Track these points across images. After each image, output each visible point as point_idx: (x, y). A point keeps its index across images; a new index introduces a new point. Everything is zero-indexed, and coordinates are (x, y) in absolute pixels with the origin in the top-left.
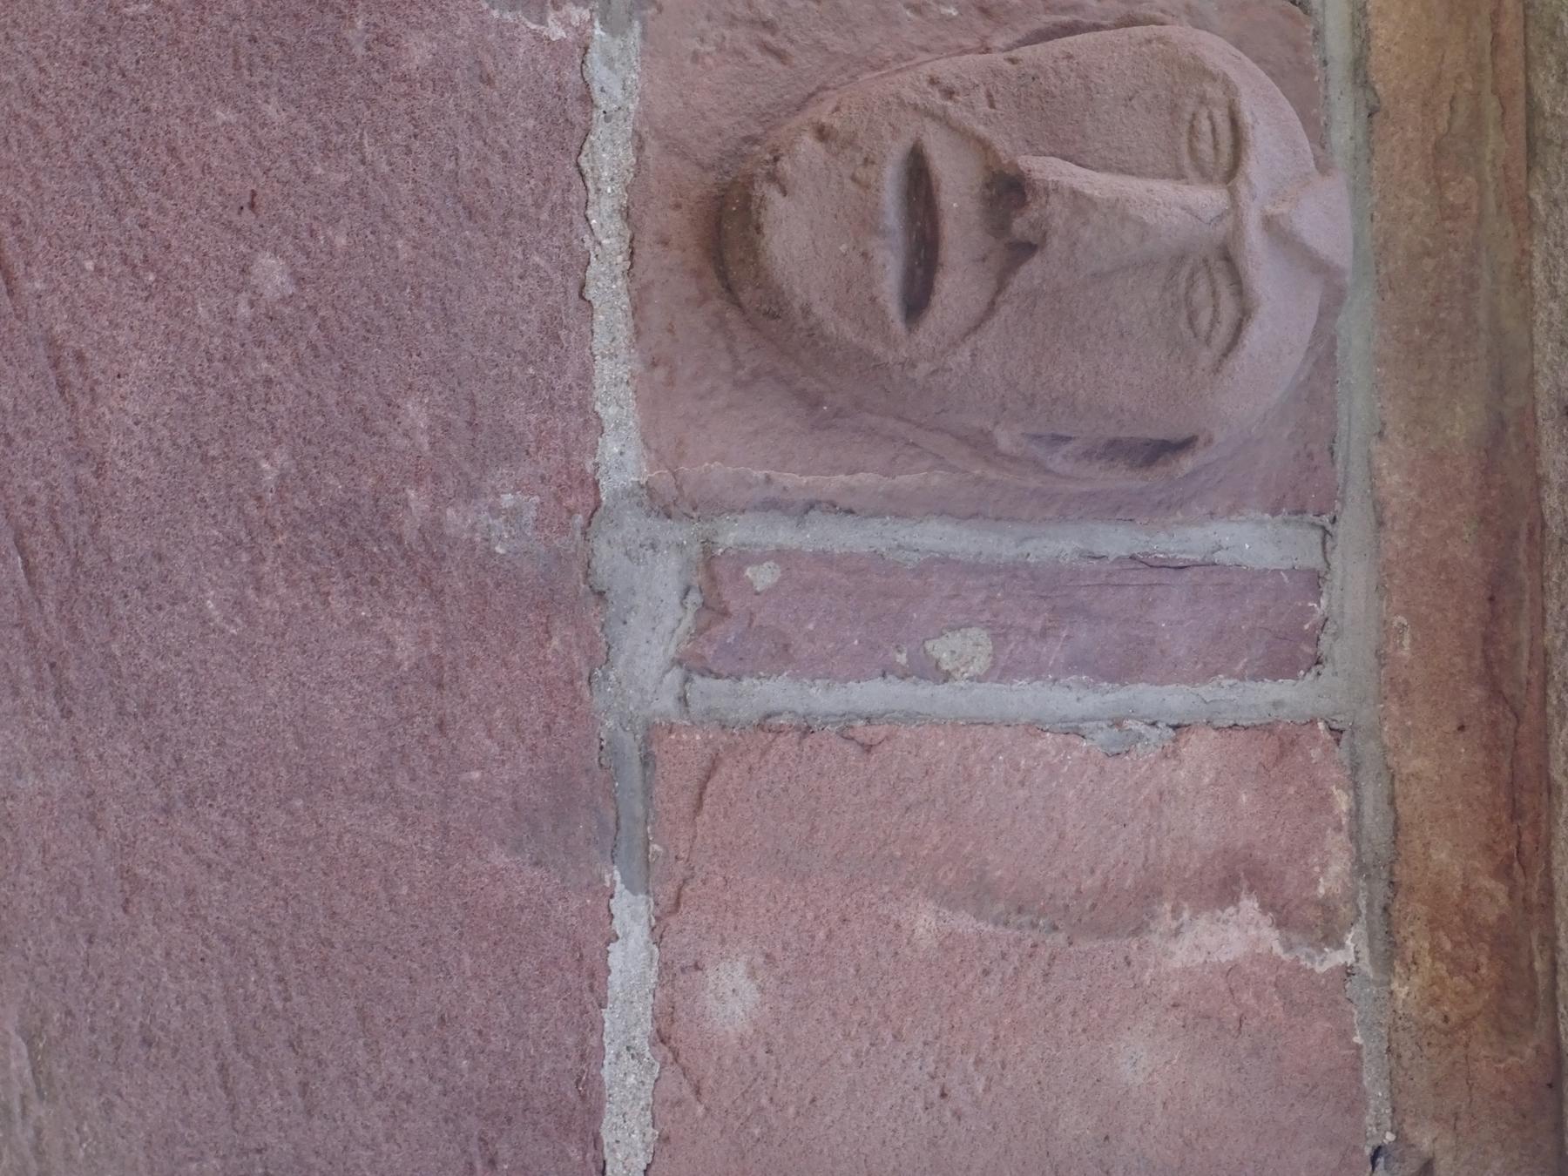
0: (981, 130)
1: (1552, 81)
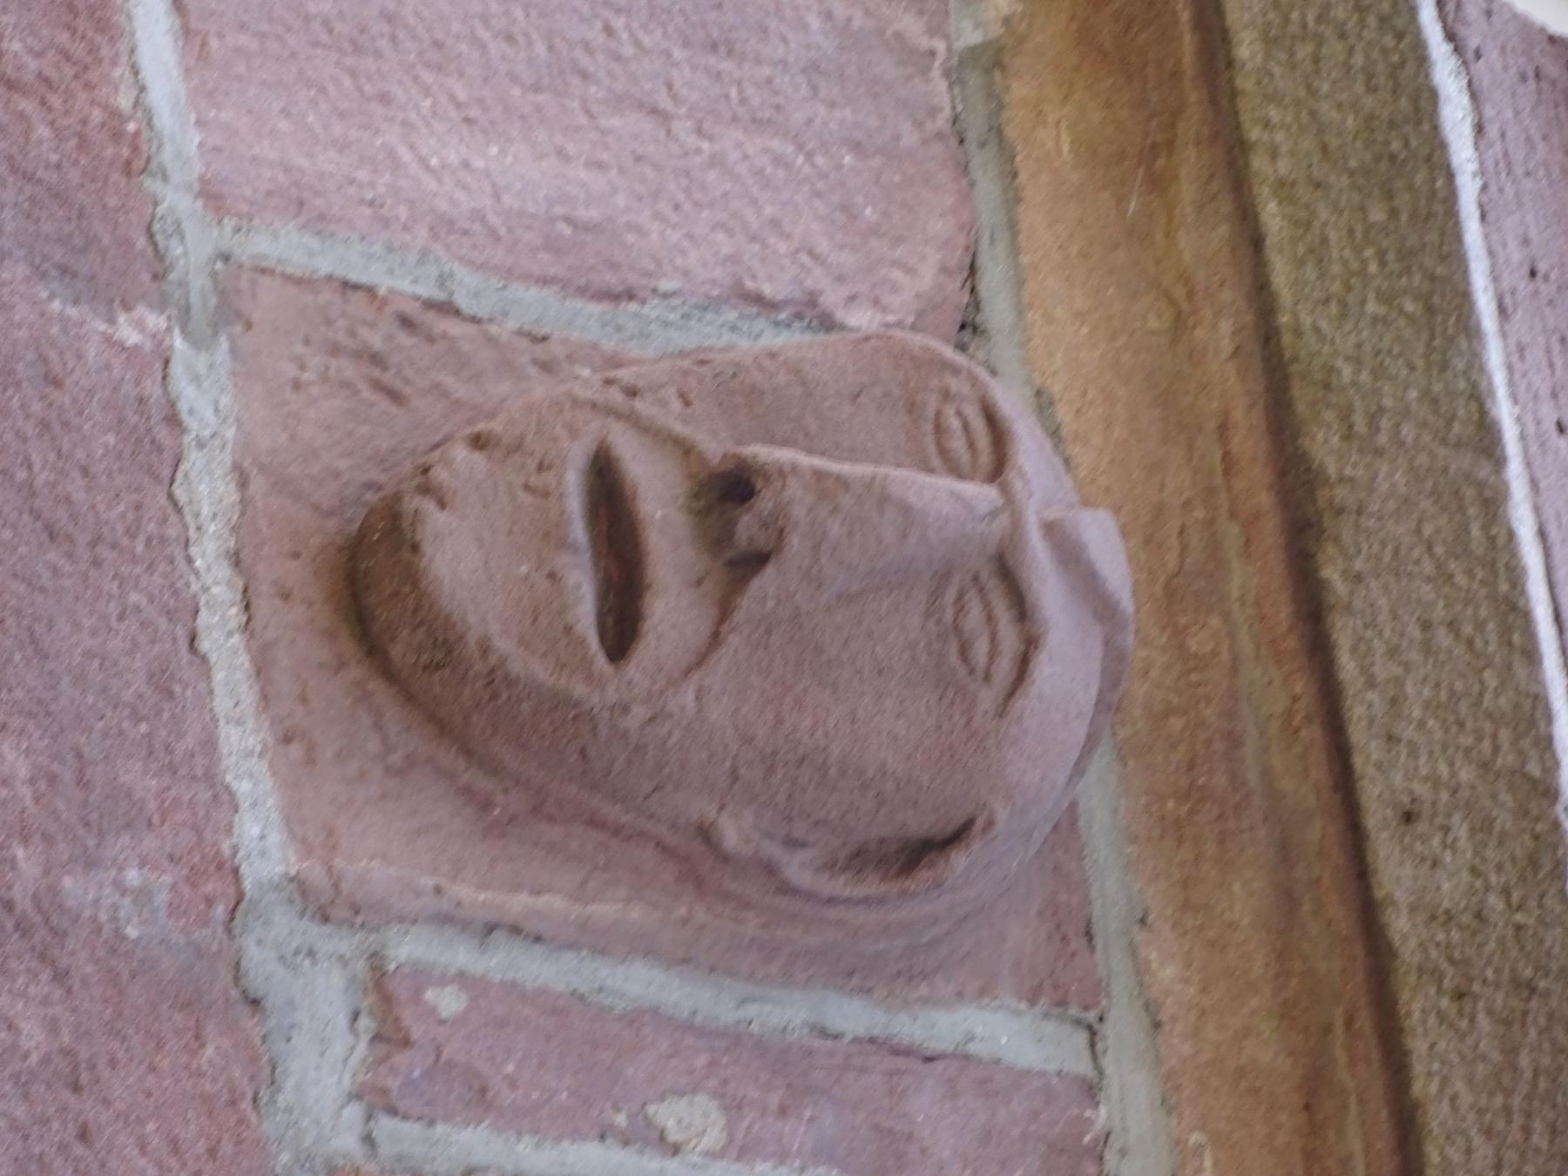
0: (679, 428)
1: (1335, 441)
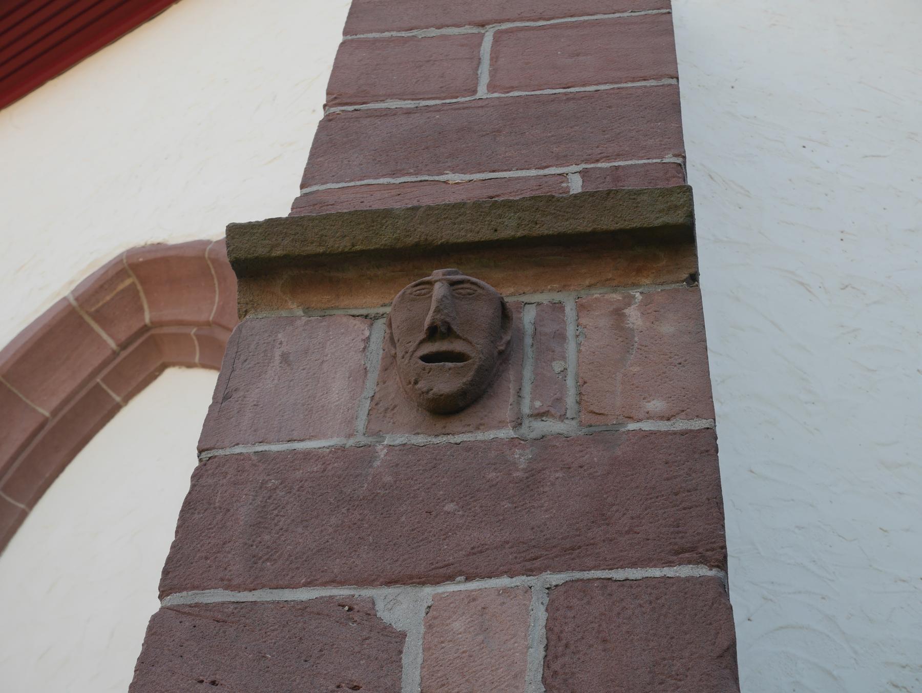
0: (417, 342)
